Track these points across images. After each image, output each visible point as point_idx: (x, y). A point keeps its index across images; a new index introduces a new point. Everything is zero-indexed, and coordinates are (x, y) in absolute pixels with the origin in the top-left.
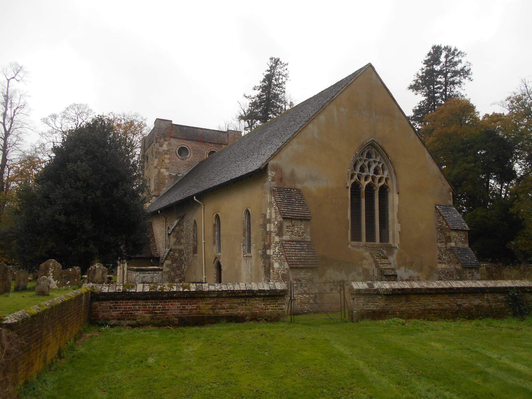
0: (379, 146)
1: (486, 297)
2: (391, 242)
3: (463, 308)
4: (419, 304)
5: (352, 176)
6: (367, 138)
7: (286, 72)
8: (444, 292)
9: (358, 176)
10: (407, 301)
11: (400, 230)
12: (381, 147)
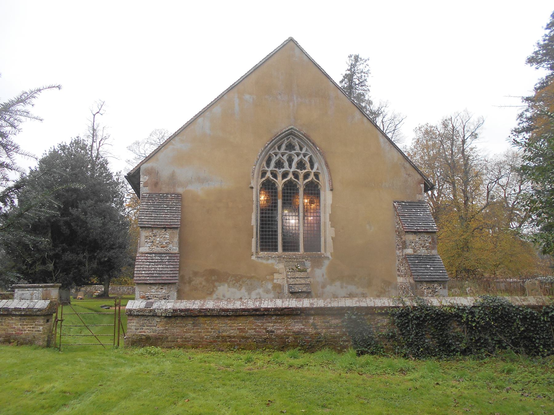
0: (302, 134)
1: (311, 321)
2: (322, 251)
3: (276, 336)
4: (212, 329)
5: (264, 174)
6: (283, 126)
7: (368, 68)
8: (246, 313)
9: (272, 173)
10: (194, 325)
11: (334, 236)
12: (304, 135)
